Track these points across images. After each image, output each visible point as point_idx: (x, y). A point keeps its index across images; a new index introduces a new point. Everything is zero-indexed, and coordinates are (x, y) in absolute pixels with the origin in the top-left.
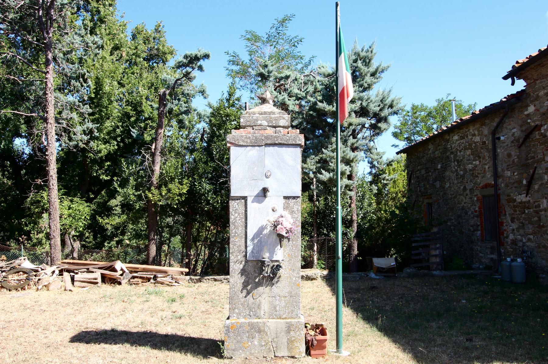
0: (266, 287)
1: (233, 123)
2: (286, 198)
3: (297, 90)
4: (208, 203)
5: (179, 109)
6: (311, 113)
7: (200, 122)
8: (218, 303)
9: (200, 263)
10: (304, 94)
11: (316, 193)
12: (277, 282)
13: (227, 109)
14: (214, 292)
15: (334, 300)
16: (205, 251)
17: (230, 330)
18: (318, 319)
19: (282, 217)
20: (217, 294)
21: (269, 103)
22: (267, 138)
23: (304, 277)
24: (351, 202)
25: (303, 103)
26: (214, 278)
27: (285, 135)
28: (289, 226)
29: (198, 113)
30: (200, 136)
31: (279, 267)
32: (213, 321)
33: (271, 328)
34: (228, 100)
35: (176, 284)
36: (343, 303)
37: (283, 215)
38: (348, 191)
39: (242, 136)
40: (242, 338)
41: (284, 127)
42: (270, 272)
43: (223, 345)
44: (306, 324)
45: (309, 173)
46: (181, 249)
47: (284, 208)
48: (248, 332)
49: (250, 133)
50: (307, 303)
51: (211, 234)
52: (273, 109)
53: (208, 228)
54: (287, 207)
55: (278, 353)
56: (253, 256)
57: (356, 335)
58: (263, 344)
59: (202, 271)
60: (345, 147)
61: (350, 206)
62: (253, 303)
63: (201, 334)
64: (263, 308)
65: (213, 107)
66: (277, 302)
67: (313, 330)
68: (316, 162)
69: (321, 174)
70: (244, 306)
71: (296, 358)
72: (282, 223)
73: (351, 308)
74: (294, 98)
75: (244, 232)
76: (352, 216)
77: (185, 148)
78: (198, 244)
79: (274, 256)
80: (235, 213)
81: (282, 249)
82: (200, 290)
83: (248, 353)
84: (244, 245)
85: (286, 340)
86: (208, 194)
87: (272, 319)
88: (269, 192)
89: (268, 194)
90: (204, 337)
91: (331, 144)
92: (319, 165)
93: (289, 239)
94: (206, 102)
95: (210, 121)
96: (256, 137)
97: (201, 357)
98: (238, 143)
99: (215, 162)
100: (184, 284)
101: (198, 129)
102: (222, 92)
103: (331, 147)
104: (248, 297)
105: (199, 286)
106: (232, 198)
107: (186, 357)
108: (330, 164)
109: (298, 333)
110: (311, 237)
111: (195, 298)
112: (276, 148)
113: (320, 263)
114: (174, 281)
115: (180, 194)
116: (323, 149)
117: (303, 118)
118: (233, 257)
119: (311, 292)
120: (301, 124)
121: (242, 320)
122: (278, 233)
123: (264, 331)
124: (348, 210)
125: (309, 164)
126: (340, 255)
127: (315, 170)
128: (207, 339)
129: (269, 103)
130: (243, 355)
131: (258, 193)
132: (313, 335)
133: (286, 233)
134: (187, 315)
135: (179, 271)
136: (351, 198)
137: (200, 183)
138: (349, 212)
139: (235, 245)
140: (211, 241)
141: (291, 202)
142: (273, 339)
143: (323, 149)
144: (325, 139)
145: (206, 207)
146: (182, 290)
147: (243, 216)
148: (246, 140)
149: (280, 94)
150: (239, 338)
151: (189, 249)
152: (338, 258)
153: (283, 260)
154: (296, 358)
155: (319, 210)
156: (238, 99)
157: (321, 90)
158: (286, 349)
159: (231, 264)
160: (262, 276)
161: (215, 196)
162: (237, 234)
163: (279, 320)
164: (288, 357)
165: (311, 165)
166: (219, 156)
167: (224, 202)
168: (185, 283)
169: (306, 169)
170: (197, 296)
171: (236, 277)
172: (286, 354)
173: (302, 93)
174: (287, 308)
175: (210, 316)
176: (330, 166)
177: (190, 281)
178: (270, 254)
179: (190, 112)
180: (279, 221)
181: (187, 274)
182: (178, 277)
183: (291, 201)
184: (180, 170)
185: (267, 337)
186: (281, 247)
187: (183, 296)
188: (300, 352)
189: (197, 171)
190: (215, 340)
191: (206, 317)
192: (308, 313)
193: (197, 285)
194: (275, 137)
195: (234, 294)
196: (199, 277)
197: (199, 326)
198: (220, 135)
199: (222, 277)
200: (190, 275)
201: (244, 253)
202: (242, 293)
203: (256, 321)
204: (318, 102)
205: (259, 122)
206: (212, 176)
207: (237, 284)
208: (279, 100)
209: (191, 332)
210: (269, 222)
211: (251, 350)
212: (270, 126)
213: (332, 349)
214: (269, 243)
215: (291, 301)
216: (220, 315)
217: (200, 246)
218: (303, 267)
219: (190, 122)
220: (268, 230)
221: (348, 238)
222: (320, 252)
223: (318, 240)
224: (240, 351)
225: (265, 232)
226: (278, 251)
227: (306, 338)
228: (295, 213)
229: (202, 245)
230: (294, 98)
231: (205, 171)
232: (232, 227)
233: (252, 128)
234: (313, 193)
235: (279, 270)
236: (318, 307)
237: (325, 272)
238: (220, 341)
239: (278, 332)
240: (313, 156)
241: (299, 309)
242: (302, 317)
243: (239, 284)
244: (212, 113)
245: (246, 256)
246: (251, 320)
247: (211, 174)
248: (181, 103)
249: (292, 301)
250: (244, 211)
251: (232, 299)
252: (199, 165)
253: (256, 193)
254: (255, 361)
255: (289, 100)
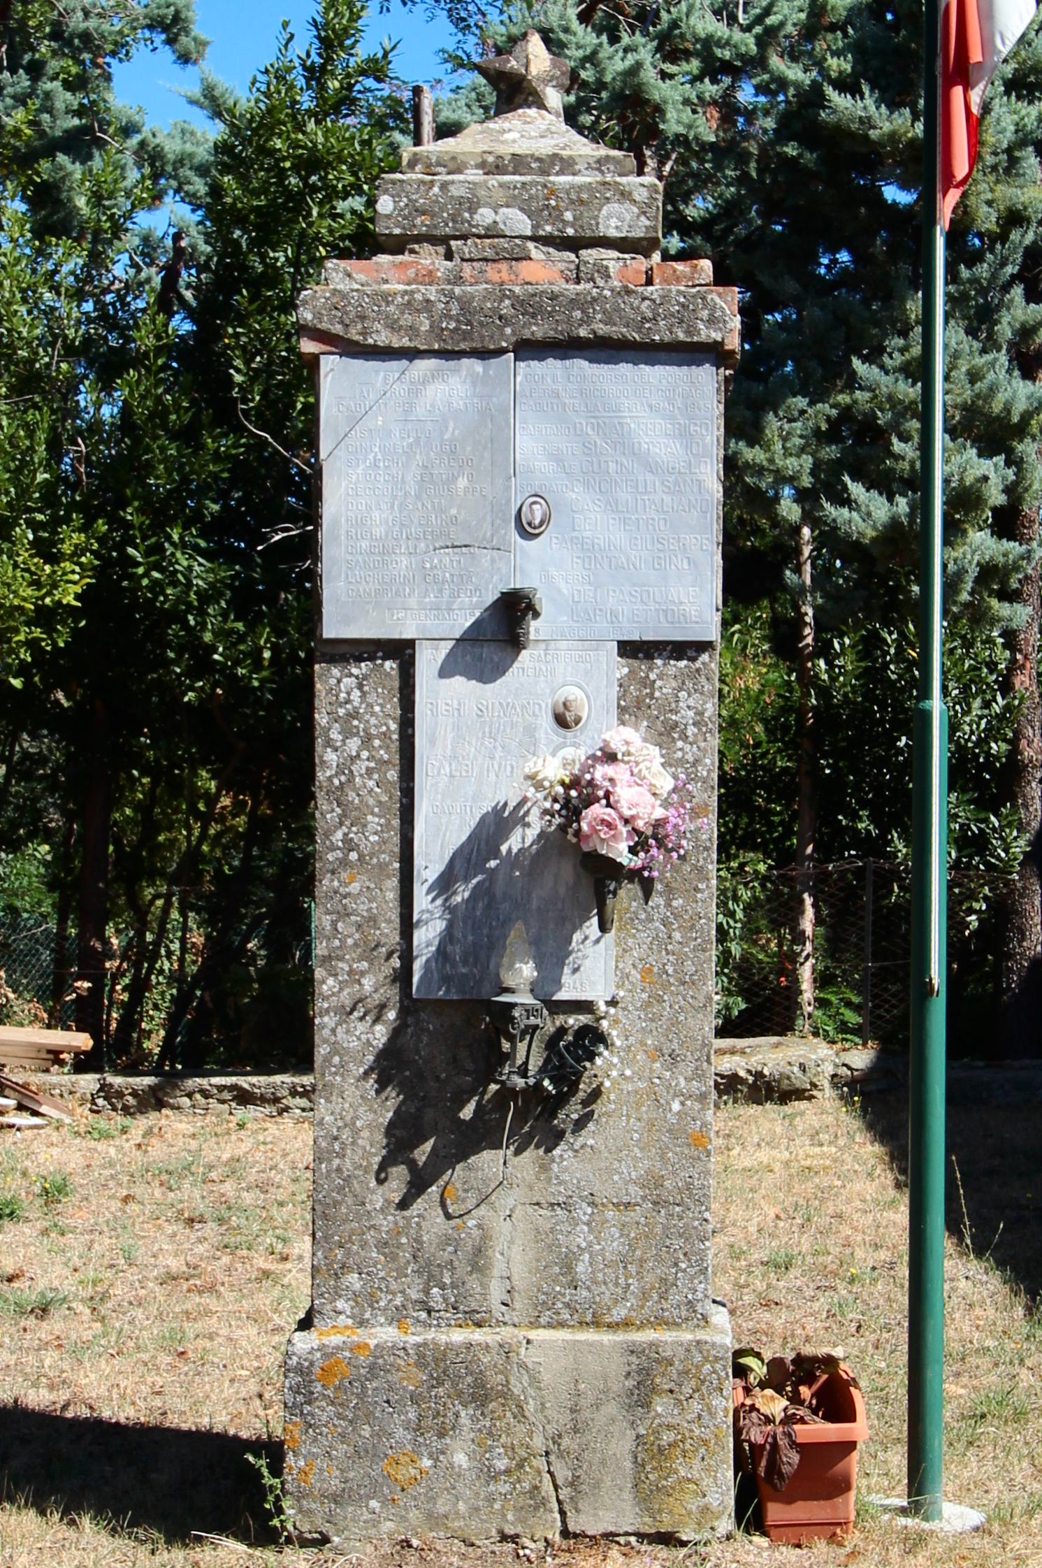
0: (518, 1152)
1: (342, 206)
2: (629, 649)
3: (709, 16)
4: (201, 664)
5: (33, 124)
6: (791, 150)
7: (158, 197)
8: (255, 1227)
9: (161, 996)
10: (749, 43)
11: (817, 609)
12: (580, 1124)
13: (311, 125)
14: (234, 1167)
15: (901, 1216)
16: (185, 928)
17: (317, 1388)
18: (812, 1325)
19: (610, 757)
20: (252, 1175)
21: (541, 105)
22: (529, 305)
23: (742, 1081)
24: (1013, 661)
25: (746, 94)
26: (234, 1087)
27: (629, 292)
28: (648, 811)
29: (143, 144)
30: (157, 281)
31: (591, 1040)
32: (224, 1332)
33: (546, 1378)
34: (315, 74)
35: (24, 1119)
36: (953, 1227)
37: (617, 746)
38: (994, 602)
39: (387, 297)
40: (383, 1433)
41: (624, 245)
42: (542, 1070)
43: (276, 1471)
44: (738, 1354)
45: (777, 499)
46: (52, 926)
47: (622, 710)
48: (415, 1399)
49: (429, 277)
50: (753, 1229)
51: (219, 835)
52: (561, 141)
53: (201, 807)
54: (639, 703)
55: (582, 1518)
56: (446, 980)
57: (1020, 1416)
58: (501, 1464)
59: (168, 1042)
60: (984, 351)
61: (1006, 687)
62: (447, 1240)
63: (158, 1402)
64: (499, 1267)
65: (230, 111)
66: (582, 1237)
67: (779, 1390)
68: (817, 432)
69: (844, 500)
70: (393, 1257)
71: (684, 1544)
72: (607, 795)
73: (1001, 1264)
74: (695, 65)
75: (397, 840)
76: (1014, 743)
77: (70, 351)
78: (149, 892)
79: (567, 978)
80: (348, 733)
81: (610, 937)
82: (157, 1150)
83: (413, 1515)
84: (394, 916)
85: (628, 1444)
86: (201, 613)
87: (550, 1326)
88: (536, 615)
89: (535, 628)
90: (173, 1421)
91: (904, 333)
92: (831, 452)
93: (647, 888)
94: (189, 82)
95: (216, 191)
96: (464, 303)
97: (156, 1535)
98: (364, 333)
99: (240, 430)
100: (67, 1120)
101: (146, 240)
102: (285, 25)
103: (902, 351)
104: (419, 1205)
105: (149, 1133)
106: (328, 649)
107: (71, 1533)
108: (897, 446)
109: (696, 1406)
110: (785, 857)
111: (126, 1199)
112: (580, 366)
113: (833, 999)
114: (12, 1103)
115: (40, 609)
116: (856, 363)
117: (744, 179)
118: (331, 981)
119: (777, 1167)
120: (730, 211)
121: (384, 1334)
122: (586, 848)
123: (505, 1394)
124: (996, 708)
125: (778, 447)
126: (937, 973)
127: (806, 481)
128: (190, 1432)
129: (541, 105)
130: (389, 1526)
131: (477, 624)
132: (780, 1417)
133: (633, 851)
134: (83, 1294)
135: (39, 1048)
136: (1011, 639)
137: (159, 549)
138: (1000, 717)
139: (345, 914)
140: (219, 872)
141: (660, 677)
142: (557, 1439)
143: (856, 363)
144: (866, 303)
145: (192, 689)
146: (55, 1151)
147: (389, 753)
148: (406, 320)
149: (614, 39)
150: (366, 1431)
151: (94, 924)
152: (926, 990)
153: (613, 1003)
154: (684, 1544)
155: (829, 705)
156: (376, 69)
157: (849, 21)
158: (627, 1495)
159: (325, 1022)
160: (494, 1087)
161: (240, 626)
162: (353, 856)
163: (590, 1335)
164: (641, 1536)
165: (787, 453)
166: (264, 395)
167: (294, 659)
168: (71, 1113)
169: (759, 471)
170: (138, 1190)
171: (352, 1092)
172: (628, 1519)
173: (737, 35)
174: (632, 1269)
175: (207, 1300)
176: (898, 458)
177: (100, 1102)
178: (538, 967)
179: (101, 144)
180: (591, 783)
181: (83, 1063)
182: (36, 1079)
183: (665, 672)
184: (41, 477)
185: (521, 1429)
186: (603, 928)
187: (62, 1189)
188: (705, 1509)
189: (141, 481)
190: (236, 1438)
191: (188, 1306)
192: (760, 1285)
193: (140, 1124)
194: (575, 302)
195: (340, 1189)
196: (149, 1081)
197: (145, 1357)
198: (272, 276)
199: (278, 1079)
200: (99, 1070)
201: (396, 962)
202: (380, 1182)
203: (458, 1336)
204: (829, 91)
205: (485, 216)
206: (225, 507)
207: (356, 1132)
208: (608, 78)
209: (103, 1391)
210: (539, 786)
211: (432, 1500)
212: (547, 241)
213: (887, 1492)
214: (535, 904)
215: (658, 1229)
216: (265, 1299)
217: (160, 902)
218: (729, 1028)
219: (97, 199)
220: (532, 834)
221: (990, 866)
222: (833, 946)
223: (823, 877)
224: (374, 1504)
225: (514, 842)
226: (589, 949)
227: (737, 1431)
228: (684, 737)
229: (168, 897)
230: (695, 65)
231: (185, 480)
232: (326, 812)
233: (441, 250)
234: (797, 608)
235: (591, 1057)
236: (816, 1253)
237: (861, 1058)
238: (257, 1446)
239: (583, 1402)
240: (800, 402)
241: (704, 1271)
242: (720, 1317)
243: (365, 1134)
244: (222, 148)
245: (403, 976)
246: (431, 1335)
247: (222, 497)
248: (49, 86)
249: (665, 1228)
250: (394, 726)
251: (325, 1216)
252: (148, 450)
253: (464, 621)
254: (455, 1559)
255: (664, 76)
